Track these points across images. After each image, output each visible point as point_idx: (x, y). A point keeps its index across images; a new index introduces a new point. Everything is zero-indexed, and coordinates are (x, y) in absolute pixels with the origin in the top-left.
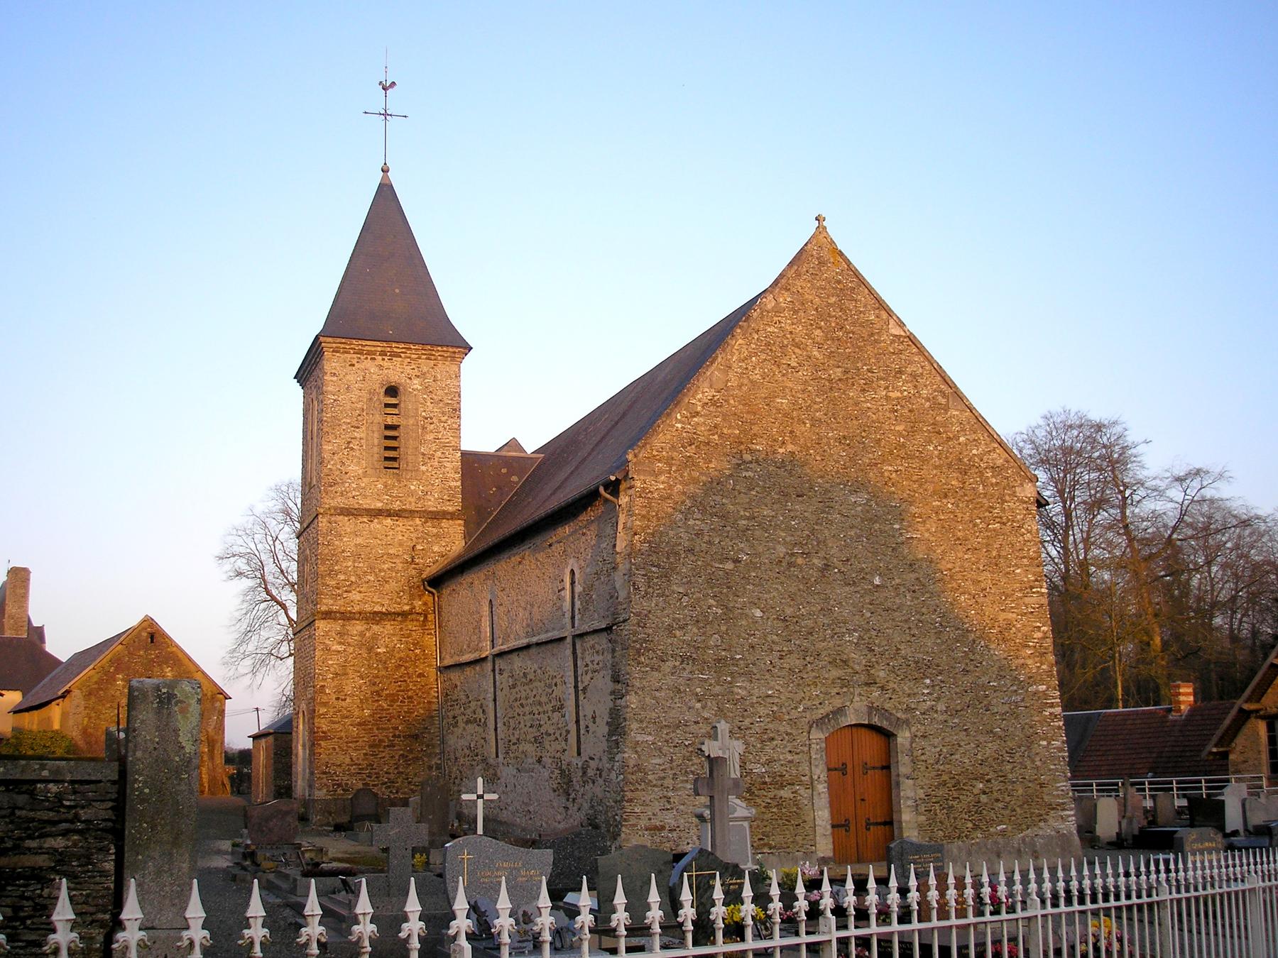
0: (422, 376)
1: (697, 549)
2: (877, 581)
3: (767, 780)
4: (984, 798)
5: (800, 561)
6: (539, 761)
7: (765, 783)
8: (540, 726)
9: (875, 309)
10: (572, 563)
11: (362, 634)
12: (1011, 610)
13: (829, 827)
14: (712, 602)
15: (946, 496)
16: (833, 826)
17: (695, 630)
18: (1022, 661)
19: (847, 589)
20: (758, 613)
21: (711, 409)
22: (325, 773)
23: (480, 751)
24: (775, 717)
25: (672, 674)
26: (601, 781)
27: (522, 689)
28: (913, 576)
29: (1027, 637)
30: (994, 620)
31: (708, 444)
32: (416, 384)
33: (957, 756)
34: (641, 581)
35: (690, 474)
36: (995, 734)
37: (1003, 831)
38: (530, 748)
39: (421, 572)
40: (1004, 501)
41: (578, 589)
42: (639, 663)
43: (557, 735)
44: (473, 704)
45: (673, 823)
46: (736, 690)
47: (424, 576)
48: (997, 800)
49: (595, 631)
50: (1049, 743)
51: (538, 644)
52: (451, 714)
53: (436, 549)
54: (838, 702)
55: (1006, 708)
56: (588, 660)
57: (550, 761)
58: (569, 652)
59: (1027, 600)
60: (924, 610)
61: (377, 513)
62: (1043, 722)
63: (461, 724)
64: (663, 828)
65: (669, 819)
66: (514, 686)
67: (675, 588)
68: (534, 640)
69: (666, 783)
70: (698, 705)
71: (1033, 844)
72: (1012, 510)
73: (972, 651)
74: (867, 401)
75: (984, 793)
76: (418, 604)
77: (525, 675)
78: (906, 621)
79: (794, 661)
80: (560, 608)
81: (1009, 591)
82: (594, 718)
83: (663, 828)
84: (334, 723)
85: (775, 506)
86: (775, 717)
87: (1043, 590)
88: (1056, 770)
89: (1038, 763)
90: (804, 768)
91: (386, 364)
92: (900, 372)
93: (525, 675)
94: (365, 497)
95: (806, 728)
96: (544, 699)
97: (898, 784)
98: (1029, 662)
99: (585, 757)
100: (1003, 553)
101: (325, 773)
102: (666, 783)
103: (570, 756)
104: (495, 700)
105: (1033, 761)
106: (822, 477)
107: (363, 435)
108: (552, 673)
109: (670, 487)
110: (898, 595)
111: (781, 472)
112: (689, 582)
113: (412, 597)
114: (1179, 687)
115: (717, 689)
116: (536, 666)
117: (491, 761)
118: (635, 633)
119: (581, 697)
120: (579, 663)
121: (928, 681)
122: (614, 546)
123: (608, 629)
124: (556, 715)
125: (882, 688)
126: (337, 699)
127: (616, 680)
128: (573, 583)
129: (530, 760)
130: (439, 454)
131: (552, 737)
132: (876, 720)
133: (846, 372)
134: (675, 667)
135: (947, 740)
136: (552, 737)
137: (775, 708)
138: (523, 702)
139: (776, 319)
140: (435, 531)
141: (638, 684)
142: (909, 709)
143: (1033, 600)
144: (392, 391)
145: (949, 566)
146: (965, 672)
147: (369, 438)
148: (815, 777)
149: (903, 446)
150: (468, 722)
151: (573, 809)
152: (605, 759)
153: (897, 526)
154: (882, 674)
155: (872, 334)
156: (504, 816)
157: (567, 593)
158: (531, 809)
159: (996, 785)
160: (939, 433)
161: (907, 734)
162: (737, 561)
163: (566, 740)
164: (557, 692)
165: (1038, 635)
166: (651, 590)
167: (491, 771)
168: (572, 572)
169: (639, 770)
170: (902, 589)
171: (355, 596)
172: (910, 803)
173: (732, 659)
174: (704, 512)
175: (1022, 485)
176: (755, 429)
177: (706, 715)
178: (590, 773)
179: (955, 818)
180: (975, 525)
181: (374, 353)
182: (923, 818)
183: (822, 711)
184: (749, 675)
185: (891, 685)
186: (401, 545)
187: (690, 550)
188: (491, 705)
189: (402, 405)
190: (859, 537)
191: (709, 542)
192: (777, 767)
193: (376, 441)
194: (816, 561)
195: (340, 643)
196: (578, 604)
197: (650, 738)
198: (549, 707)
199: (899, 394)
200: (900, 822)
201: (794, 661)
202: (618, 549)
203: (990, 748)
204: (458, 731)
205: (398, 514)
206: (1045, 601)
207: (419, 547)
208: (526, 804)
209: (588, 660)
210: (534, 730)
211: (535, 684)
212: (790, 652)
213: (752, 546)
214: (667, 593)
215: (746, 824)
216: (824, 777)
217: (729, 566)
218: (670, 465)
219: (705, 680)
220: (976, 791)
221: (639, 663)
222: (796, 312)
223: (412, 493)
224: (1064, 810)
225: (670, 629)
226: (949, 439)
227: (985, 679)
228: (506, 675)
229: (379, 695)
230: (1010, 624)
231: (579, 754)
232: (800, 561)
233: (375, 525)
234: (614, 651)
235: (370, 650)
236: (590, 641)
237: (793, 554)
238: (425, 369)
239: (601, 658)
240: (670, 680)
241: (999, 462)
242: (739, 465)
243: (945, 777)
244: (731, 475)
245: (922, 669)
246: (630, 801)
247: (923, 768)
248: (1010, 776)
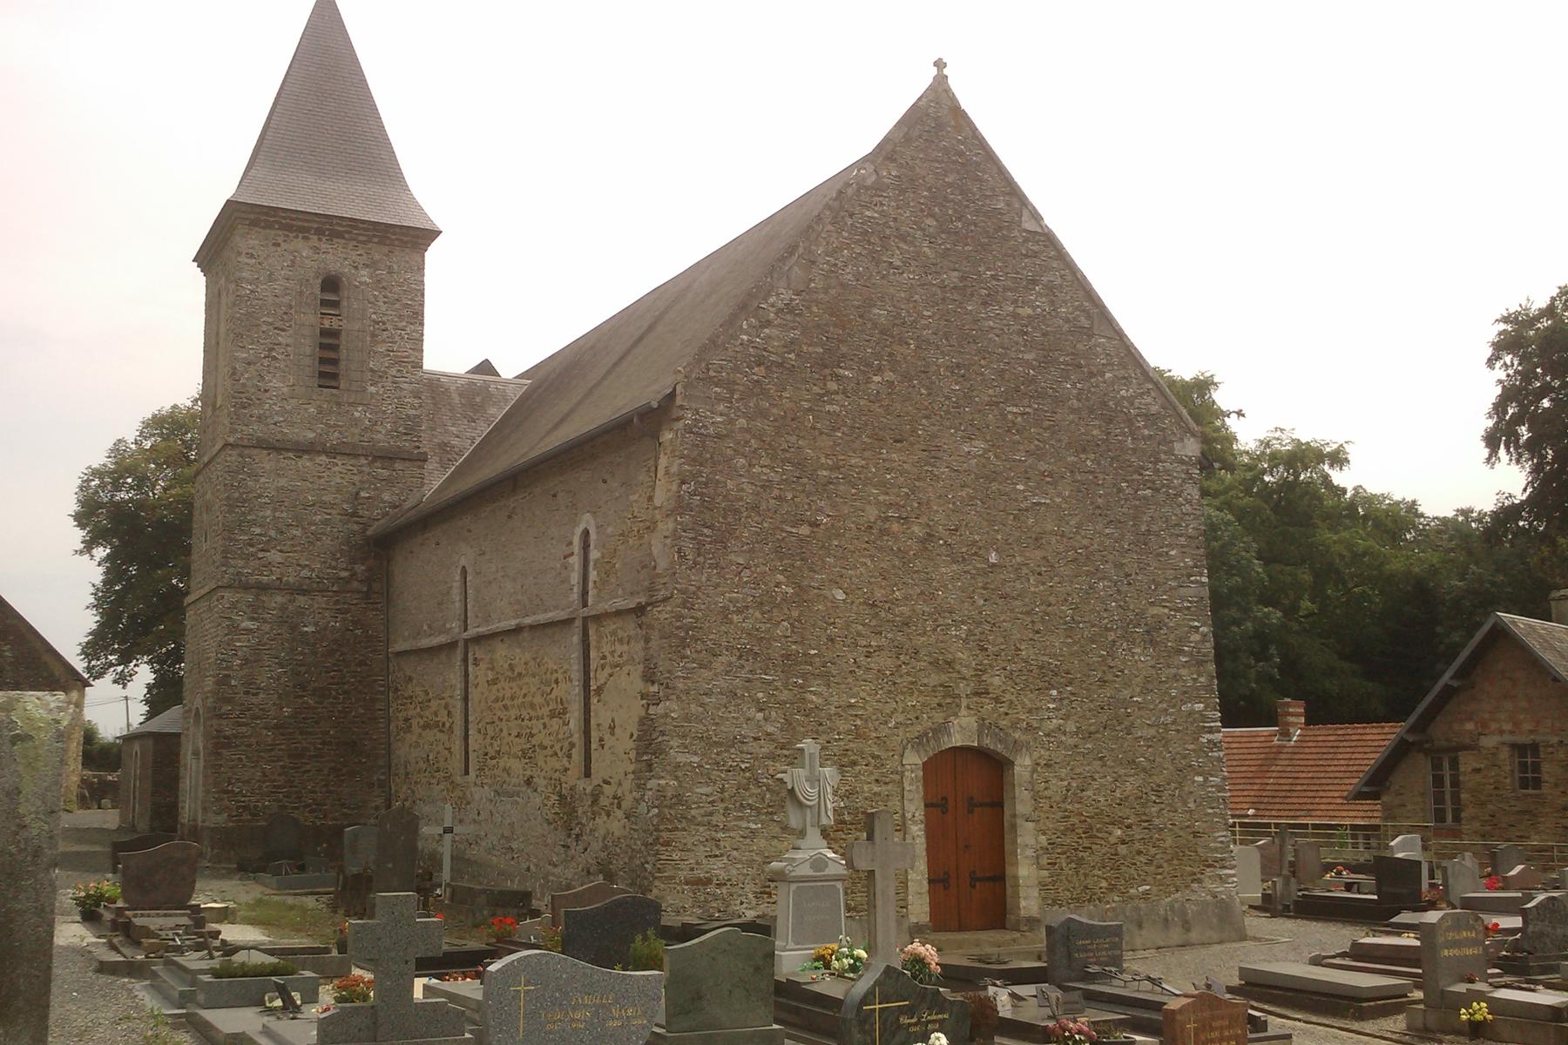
0: (372, 265)
1: (764, 506)
2: (993, 558)
3: (847, 818)
4: (1122, 849)
5: (895, 527)
6: (529, 782)
7: (844, 822)
8: (532, 735)
9: (1004, 194)
10: (587, 521)
11: (283, 608)
12: (1160, 603)
13: (925, 883)
14: (780, 577)
15: (1084, 451)
16: (930, 882)
17: (758, 614)
18: (1174, 671)
19: (955, 567)
20: (840, 595)
21: (788, 317)
22: (227, 792)
23: (442, 764)
24: (858, 735)
25: (727, 673)
26: (620, 814)
27: (506, 685)
28: (1038, 554)
29: (1181, 640)
30: (1141, 615)
31: (781, 365)
32: (364, 276)
33: (1089, 793)
34: (688, 547)
35: (757, 406)
36: (1138, 765)
37: (1146, 893)
38: (516, 765)
39: (366, 526)
40: (1158, 460)
41: (594, 554)
42: (683, 657)
43: (557, 748)
44: (434, 704)
45: (723, 875)
46: (809, 696)
47: (369, 533)
48: (1139, 853)
49: (619, 613)
50: (1206, 780)
51: (532, 627)
52: (401, 715)
53: (386, 497)
54: (939, 717)
55: (1152, 731)
56: (606, 649)
57: (544, 782)
58: (576, 639)
59: (1182, 591)
60: (1052, 599)
61: (303, 449)
62: (1200, 751)
63: (416, 730)
64: (708, 881)
65: (717, 868)
66: (494, 682)
67: (732, 557)
68: (528, 621)
69: (714, 819)
70: (760, 716)
71: (1183, 913)
72: (1167, 471)
73: (1111, 655)
74: (989, 318)
75: (1123, 842)
76: (359, 568)
77: (512, 667)
78: (1028, 613)
79: (885, 661)
80: (566, 580)
81: (1161, 579)
82: (612, 728)
83: (708, 881)
84: (240, 725)
85: (867, 454)
86: (858, 735)
87: (1204, 579)
88: (1215, 814)
89: (1192, 805)
90: (895, 803)
91: (324, 246)
92: (1034, 282)
93: (512, 667)
94: (292, 424)
95: (899, 749)
96: (538, 700)
97: (1014, 827)
98: (1183, 672)
99: (596, 779)
100: (1155, 528)
101: (227, 792)
102: (714, 819)
103: (573, 778)
104: (466, 699)
105: (1185, 803)
106: (927, 417)
107: (289, 341)
108: (551, 666)
109: (731, 422)
110: (1019, 578)
111: (875, 407)
112: (751, 551)
113: (353, 561)
114: (1288, 705)
115: (785, 695)
116: (528, 656)
117: (458, 779)
118: (679, 617)
119: (594, 700)
120: (593, 654)
121: (1054, 692)
122: (650, 498)
123: (640, 610)
124: (555, 724)
125: (997, 700)
126: (247, 693)
127: (649, 678)
128: (586, 547)
129: (514, 781)
130: (393, 371)
131: (549, 752)
132: (988, 742)
133: (963, 279)
134: (730, 664)
135: (1078, 770)
136: (549, 752)
137: (859, 722)
138: (509, 703)
139: (876, 199)
140: (385, 473)
141: (680, 686)
142: (1029, 728)
143: (1191, 591)
144: (331, 284)
145: (1085, 542)
146: (1103, 682)
147: (300, 344)
148: (909, 816)
149: (1033, 380)
150: (426, 726)
151: (576, 849)
152: (628, 784)
153: (1020, 487)
154: (996, 681)
155: (1001, 228)
156: (474, 853)
157: (575, 561)
158: (515, 846)
159: (1137, 833)
160: (1080, 366)
161: (1028, 762)
162: (815, 524)
163: (569, 756)
164: (558, 692)
165: (1196, 637)
166: (701, 559)
167: (458, 793)
168: (586, 533)
169: (680, 803)
170: (1025, 570)
171: (274, 556)
172: (1030, 852)
173: (805, 654)
174: (773, 458)
175: (1182, 440)
176: (844, 349)
177: (770, 729)
178: (604, 801)
179: (1086, 875)
180: (1120, 490)
181: (307, 230)
182: (1046, 873)
183: (919, 728)
184: (826, 677)
185: (1008, 697)
186: (338, 491)
187: (755, 508)
188: (459, 705)
189: (344, 303)
190: (972, 498)
191: (778, 498)
192: (860, 802)
193: (308, 351)
194: (916, 529)
195: (253, 619)
196: (593, 575)
197: (696, 759)
198: (546, 711)
199: (1030, 311)
200: (1016, 878)
201: (885, 661)
202: (657, 502)
203: (1131, 785)
204: (411, 738)
205: (333, 453)
206: (1206, 592)
207: (363, 494)
208: (508, 839)
209: (606, 649)
210: (522, 740)
211: (526, 679)
212: (880, 648)
213: (834, 506)
214: (722, 563)
215: (839, 885)
216: (920, 815)
217: (805, 530)
218: (732, 392)
219: (770, 683)
220: (1112, 840)
221: (683, 657)
222: (903, 192)
223: (356, 422)
224: (1224, 867)
225: (725, 613)
226: (1092, 375)
227: (1126, 693)
228: (483, 666)
229: (304, 688)
230: (1160, 623)
231: (588, 774)
232: (895, 527)
233: (305, 462)
234: (647, 640)
235: (294, 628)
236: (610, 626)
237: (887, 519)
238: (377, 257)
239: (625, 647)
240: (722, 683)
241: (1154, 409)
242: (822, 395)
243: (1075, 820)
244: (810, 410)
245: (1047, 677)
246: (667, 844)
247: (1047, 807)
248: (1156, 821)
